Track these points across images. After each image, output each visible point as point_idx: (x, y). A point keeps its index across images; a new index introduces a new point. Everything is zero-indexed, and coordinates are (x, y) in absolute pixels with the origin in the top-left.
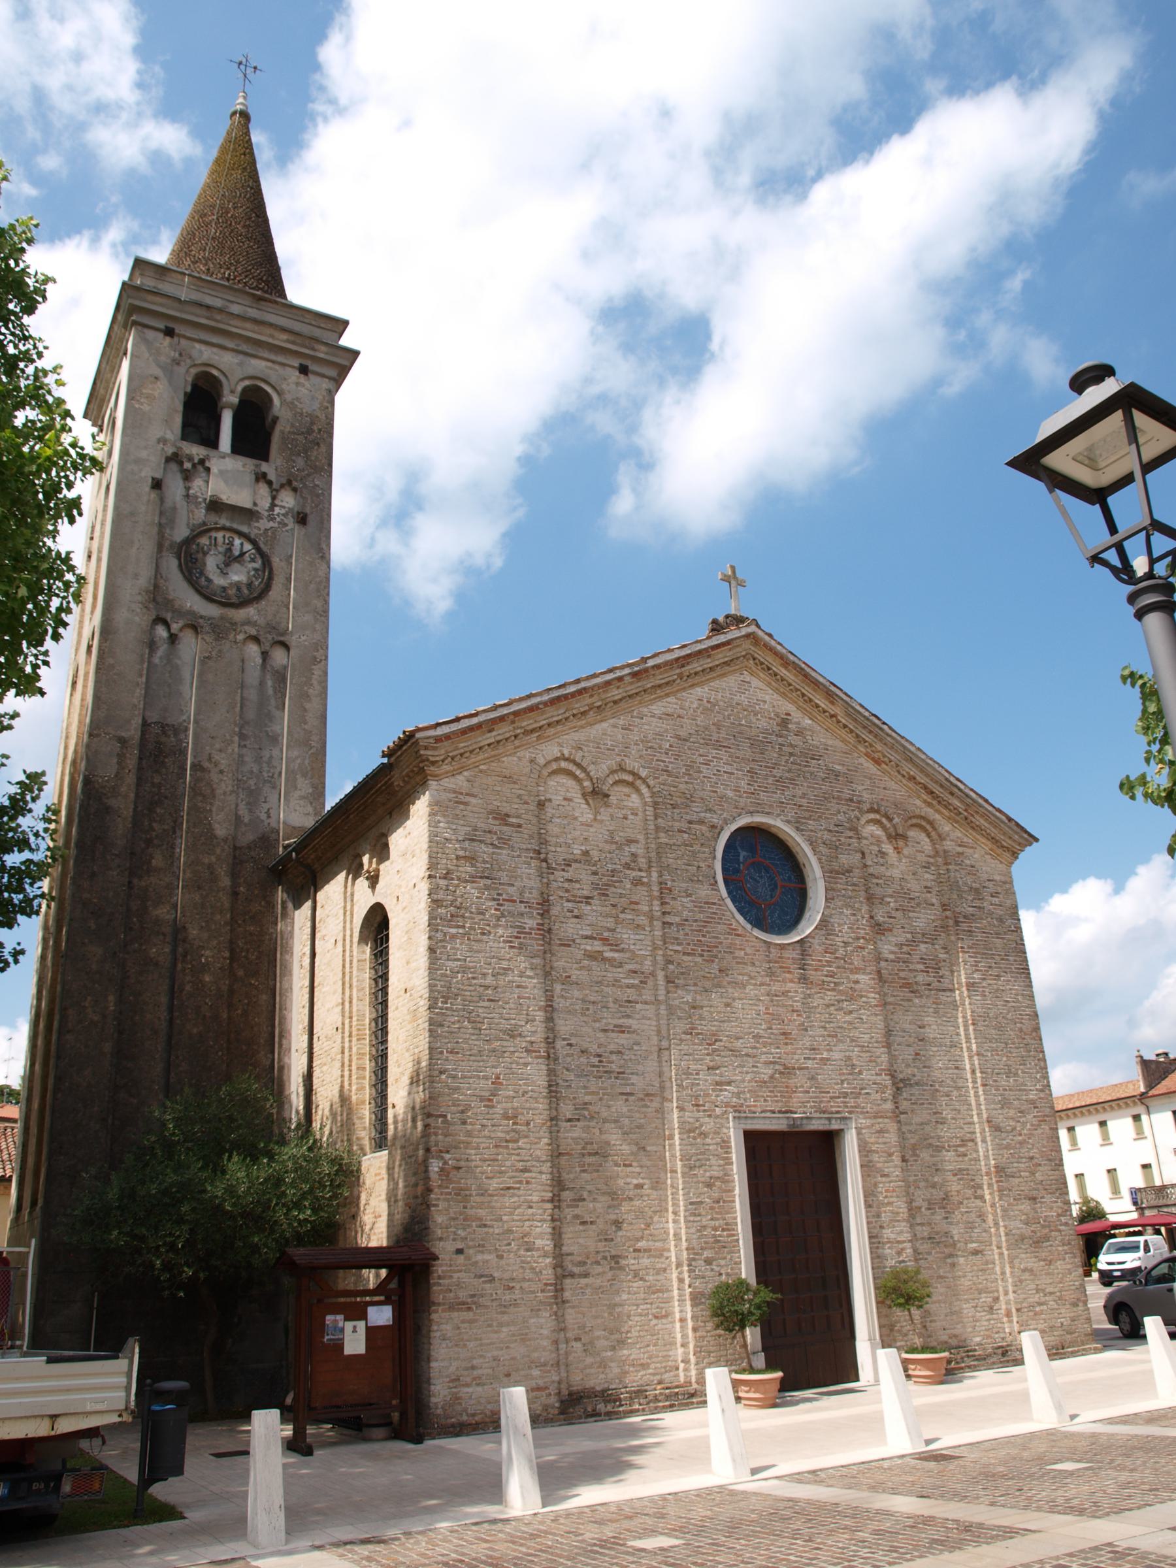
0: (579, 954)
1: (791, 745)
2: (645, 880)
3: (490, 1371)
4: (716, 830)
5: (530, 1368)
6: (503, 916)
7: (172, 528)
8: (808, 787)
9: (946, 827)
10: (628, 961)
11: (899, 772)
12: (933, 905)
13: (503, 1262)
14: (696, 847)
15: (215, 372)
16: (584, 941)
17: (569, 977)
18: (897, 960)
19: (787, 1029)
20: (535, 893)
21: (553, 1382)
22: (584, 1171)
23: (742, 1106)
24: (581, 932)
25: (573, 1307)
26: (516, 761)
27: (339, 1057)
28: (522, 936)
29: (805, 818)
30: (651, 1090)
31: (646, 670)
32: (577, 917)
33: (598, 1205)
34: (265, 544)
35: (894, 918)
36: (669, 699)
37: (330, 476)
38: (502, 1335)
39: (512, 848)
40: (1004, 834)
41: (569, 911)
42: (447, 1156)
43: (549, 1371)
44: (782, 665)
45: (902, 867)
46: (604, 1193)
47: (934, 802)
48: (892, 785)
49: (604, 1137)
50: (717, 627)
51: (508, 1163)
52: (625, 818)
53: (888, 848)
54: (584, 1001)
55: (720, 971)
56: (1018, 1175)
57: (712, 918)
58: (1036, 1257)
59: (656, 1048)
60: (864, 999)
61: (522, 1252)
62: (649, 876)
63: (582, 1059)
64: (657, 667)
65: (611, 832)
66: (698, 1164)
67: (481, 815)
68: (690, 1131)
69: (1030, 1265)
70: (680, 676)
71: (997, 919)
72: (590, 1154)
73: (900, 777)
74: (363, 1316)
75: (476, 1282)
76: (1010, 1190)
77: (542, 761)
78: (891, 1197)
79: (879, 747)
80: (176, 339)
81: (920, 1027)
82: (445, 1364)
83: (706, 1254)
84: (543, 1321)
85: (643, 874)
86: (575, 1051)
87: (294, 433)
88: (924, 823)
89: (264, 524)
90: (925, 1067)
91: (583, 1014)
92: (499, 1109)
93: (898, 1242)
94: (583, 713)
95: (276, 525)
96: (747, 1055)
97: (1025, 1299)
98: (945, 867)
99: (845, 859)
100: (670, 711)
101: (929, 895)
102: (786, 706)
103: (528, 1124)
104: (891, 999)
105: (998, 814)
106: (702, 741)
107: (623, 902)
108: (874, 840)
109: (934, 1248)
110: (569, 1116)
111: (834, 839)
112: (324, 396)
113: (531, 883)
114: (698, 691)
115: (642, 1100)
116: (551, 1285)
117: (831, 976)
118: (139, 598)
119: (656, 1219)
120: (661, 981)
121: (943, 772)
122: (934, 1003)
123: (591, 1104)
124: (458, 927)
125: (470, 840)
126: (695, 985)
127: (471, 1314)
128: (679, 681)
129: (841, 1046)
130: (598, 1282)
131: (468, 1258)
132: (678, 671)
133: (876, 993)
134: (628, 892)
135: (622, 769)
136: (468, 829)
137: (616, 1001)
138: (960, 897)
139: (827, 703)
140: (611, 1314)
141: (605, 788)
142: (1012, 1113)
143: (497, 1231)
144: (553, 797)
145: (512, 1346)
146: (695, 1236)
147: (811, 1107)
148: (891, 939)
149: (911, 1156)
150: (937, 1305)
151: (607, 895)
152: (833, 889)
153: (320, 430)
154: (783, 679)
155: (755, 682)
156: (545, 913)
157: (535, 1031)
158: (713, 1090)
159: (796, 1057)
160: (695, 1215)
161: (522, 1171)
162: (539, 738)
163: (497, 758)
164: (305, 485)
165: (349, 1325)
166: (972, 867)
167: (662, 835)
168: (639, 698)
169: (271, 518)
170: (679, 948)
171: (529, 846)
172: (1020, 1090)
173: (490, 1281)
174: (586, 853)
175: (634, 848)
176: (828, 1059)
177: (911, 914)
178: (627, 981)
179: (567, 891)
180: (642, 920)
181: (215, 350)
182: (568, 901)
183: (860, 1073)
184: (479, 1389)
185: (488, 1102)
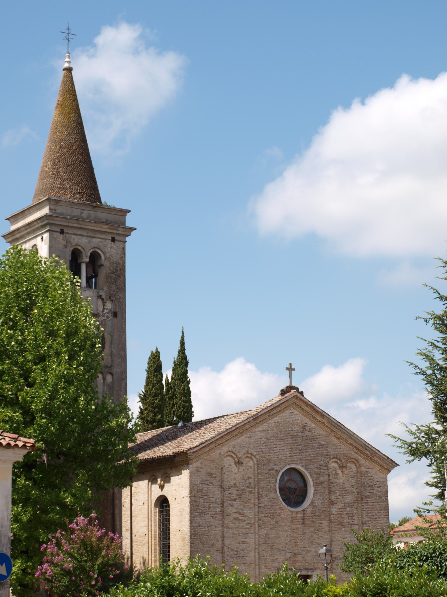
0: (232, 518)
1: (306, 436)
2: (253, 491)
4: (277, 472)
9: (363, 462)
14: (271, 479)
15: (79, 248)
16: (233, 514)
18: (338, 514)
20: (220, 500)
26: (214, 455)
27: (147, 544)
30: (252, 562)
31: (258, 417)
32: (232, 506)
36: (264, 424)
37: (125, 292)
39: (213, 485)
40: (386, 463)
45: (344, 479)
47: (359, 453)
48: (344, 447)
50: (283, 392)
53: (339, 472)
54: (233, 534)
59: (254, 548)
62: (255, 490)
64: (262, 415)
73: (346, 444)
77: (223, 453)
80: (65, 234)
85: (253, 489)
88: (354, 460)
91: (232, 538)
94: (237, 435)
98: (360, 478)
99: (322, 478)
100: (264, 429)
101: (353, 489)
104: (333, 529)
105: (384, 456)
107: (246, 500)
112: (121, 252)
113: (219, 497)
120: (257, 527)
126: (268, 527)
135: (248, 452)
137: (242, 533)
138: (365, 489)
144: (226, 465)
148: (337, 507)
151: (241, 498)
152: (317, 490)
154: (305, 411)
155: (295, 412)
156: (222, 506)
162: (222, 446)
164: (116, 298)
166: (371, 477)
167: (260, 476)
169: (103, 315)
170: (263, 515)
174: (235, 484)
177: (345, 497)
179: (229, 497)
180: (252, 505)
181: (79, 237)
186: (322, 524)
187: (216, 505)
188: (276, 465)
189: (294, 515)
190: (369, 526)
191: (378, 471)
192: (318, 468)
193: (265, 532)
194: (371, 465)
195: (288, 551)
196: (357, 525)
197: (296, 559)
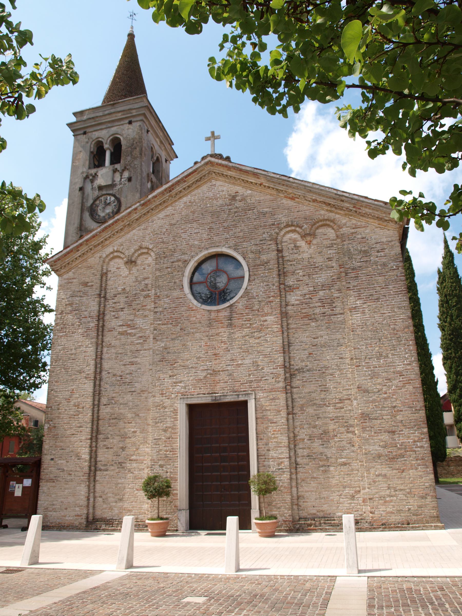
0: (116, 333)
1: (236, 207)
5: (75, 507)
6: (81, 324)
8: (245, 226)
11: (306, 200)
12: (333, 267)
13: (68, 464)
15: (100, 139)
19: (217, 352)
23: (187, 392)
25: (100, 483)
32: (116, 318)
33: (115, 441)
36: (168, 209)
40: (385, 213)
42: (51, 423)
44: (228, 170)
47: (333, 209)
49: (120, 411)
51: (74, 424)
52: (144, 269)
56: (381, 417)
58: (390, 467)
60: (269, 329)
61: (76, 460)
65: (136, 277)
66: (160, 421)
68: (157, 406)
69: (383, 473)
70: (170, 196)
71: (381, 265)
72: (113, 419)
74: (22, 482)
75: (57, 471)
76: (371, 427)
78: (277, 434)
79: (290, 191)
81: (314, 338)
83: (160, 463)
84: (82, 488)
86: (110, 375)
89: (118, 187)
90: (315, 360)
91: (116, 359)
92: (72, 403)
93: (279, 458)
96: (192, 368)
97: (377, 492)
103: (83, 408)
105: (376, 203)
107: (139, 307)
108: (291, 242)
109: (311, 461)
110: (105, 403)
114: (185, 199)
115: (139, 393)
117: (248, 321)
119: (141, 446)
122: (326, 323)
126: (167, 338)
127: (54, 484)
129: (251, 356)
131: (55, 462)
132: (168, 194)
137: (131, 351)
139: (256, 179)
140: (116, 487)
141: (133, 259)
142: (379, 380)
143: (67, 451)
147: (228, 390)
148: (300, 292)
149: (299, 411)
150: (310, 493)
155: (218, 183)
157: (90, 370)
158: (171, 386)
159: (221, 365)
160: (156, 445)
162: (103, 247)
163: (86, 260)
165: (17, 485)
169: (121, 184)
170: (160, 322)
172: (388, 366)
174: (124, 289)
175: (146, 282)
176: (241, 364)
177: (314, 276)
181: (100, 131)
183: (263, 369)
184: (55, 513)
185: (68, 400)
186: (266, 321)
187: (89, 319)
188: (184, 254)
189: (213, 315)
191: (377, 228)
192: (257, 245)
193: (163, 345)
194: (361, 222)
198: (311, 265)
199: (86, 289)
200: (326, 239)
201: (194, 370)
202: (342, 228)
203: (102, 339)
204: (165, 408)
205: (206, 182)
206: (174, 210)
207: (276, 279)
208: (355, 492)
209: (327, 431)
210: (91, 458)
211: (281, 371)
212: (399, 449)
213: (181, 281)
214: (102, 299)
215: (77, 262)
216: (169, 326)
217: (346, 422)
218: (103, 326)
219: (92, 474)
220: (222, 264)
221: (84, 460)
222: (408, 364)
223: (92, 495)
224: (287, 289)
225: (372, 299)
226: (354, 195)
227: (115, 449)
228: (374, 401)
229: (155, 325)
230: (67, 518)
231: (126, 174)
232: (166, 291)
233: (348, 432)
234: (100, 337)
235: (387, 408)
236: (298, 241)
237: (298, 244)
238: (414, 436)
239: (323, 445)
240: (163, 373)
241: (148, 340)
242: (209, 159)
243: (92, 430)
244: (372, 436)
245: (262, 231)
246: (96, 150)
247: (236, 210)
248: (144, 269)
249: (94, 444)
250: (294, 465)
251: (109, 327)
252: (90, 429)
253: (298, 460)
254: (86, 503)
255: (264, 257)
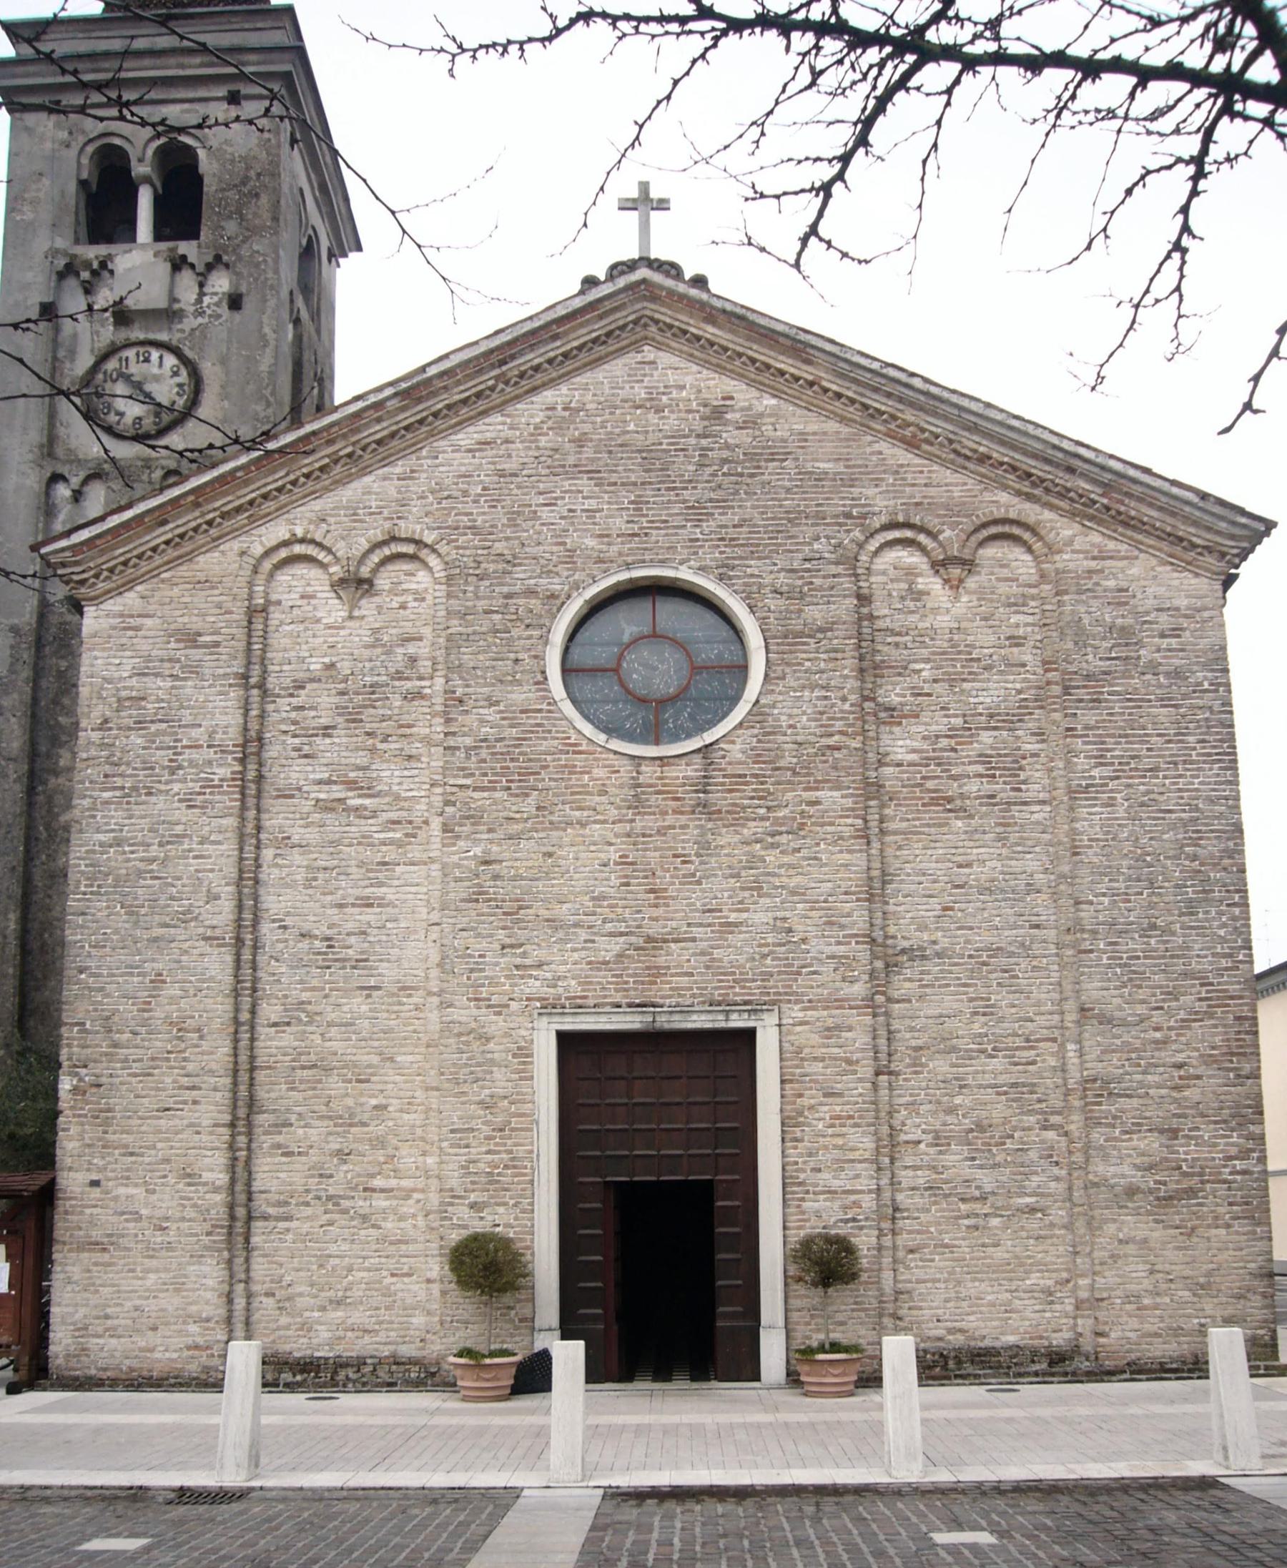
1: (727, 446)
2: (428, 691)
3: (129, 1322)
7: (73, 360)
8: (753, 507)
9: (1063, 529)
10: (385, 808)
12: (1024, 665)
15: (117, 141)
16: (316, 788)
17: (289, 838)
21: (218, 1341)
22: (292, 1089)
24: (311, 776)
25: (265, 1256)
28: (208, 791)
29: (741, 558)
32: (306, 756)
34: (191, 349)
35: (929, 695)
38: (148, 1283)
41: (295, 749)
42: (83, 1071)
43: (213, 1329)
46: (322, 1118)
52: (403, 606)
55: (538, 808)
57: (532, 732)
58: (1157, 1221)
63: (300, 945)
65: (375, 631)
67: (158, 640)
69: (1140, 1235)
71: (1167, 674)
72: (303, 1068)
73: (960, 460)
75: (115, 1219)
79: (909, 415)
81: (960, 866)
82: (71, 1309)
83: (473, 1197)
87: (223, 190)
89: (190, 323)
90: (959, 928)
95: (206, 320)
102: (718, 385)
105: (1175, 490)
106: (544, 472)
109: (935, 1203)
110: (274, 1018)
111: (800, 582)
114: (548, 396)
115: (393, 995)
116: (222, 1227)
117: (760, 798)
118: (30, 457)
121: (1046, 436)
122: (997, 824)
123: (310, 1003)
124: (115, 789)
125: (139, 674)
126: (490, 831)
127: (106, 1256)
128: (501, 386)
130: (306, 1227)
133: (856, 817)
134: (396, 711)
136: (138, 660)
139: (799, 364)
141: (365, 571)
143: (147, 1160)
145: (161, 1295)
146: (456, 1174)
149: (909, 1066)
150: (929, 1285)
153: (259, 175)
155: (665, 358)
157: (222, 914)
158: (507, 977)
161: (188, 1088)
162: (252, 520)
163: (189, 557)
168: (424, 429)
169: (200, 313)
170: (468, 782)
171: (228, 670)
172: (1172, 957)
173: (136, 1220)
175: (411, 649)
177: (966, 685)
178: (382, 836)
179: (295, 723)
182: (295, 736)
184: (114, 1341)
186: (817, 803)
189: (649, 773)
190: (1111, 803)
193: (478, 851)
195: (609, 927)
196: (1043, 802)
197: (661, 961)
198: (959, 653)
199: (196, 654)
200: (1007, 580)
201: (583, 934)
202: (1060, 552)
203: (258, 819)
204: (488, 1040)
205: (621, 351)
206: (512, 428)
207: (852, 683)
208: (1056, 1282)
209: (985, 1122)
210: (233, 1181)
211: (863, 952)
212: (1185, 1174)
213: (539, 658)
214: (255, 692)
215: (158, 560)
216: (498, 795)
217: (1040, 1101)
218: (260, 778)
219: (239, 1227)
220: (671, 614)
221: (210, 1187)
222: (1225, 956)
223: (240, 1288)
224: (882, 715)
225: (1136, 769)
226: (1112, 457)
227: (314, 1156)
228: (1128, 1048)
229: (449, 789)
230: (157, 1355)
231: (221, 283)
232: (486, 685)
233: (1045, 1128)
234: (251, 814)
235: (1162, 1069)
236: (920, 575)
237: (922, 584)
238: (1227, 1144)
239: (973, 1159)
240: (478, 935)
241: (422, 835)
242: (642, 273)
243: (235, 1100)
244: (1115, 1139)
245: (810, 532)
246: (96, 174)
247: (725, 454)
248: (403, 606)
249: (242, 1140)
250: (890, 1211)
251: (281, 783)
252: (228, 1095)
253: (900, 1197)
254: (222, 1312)
255: (815, 614)
